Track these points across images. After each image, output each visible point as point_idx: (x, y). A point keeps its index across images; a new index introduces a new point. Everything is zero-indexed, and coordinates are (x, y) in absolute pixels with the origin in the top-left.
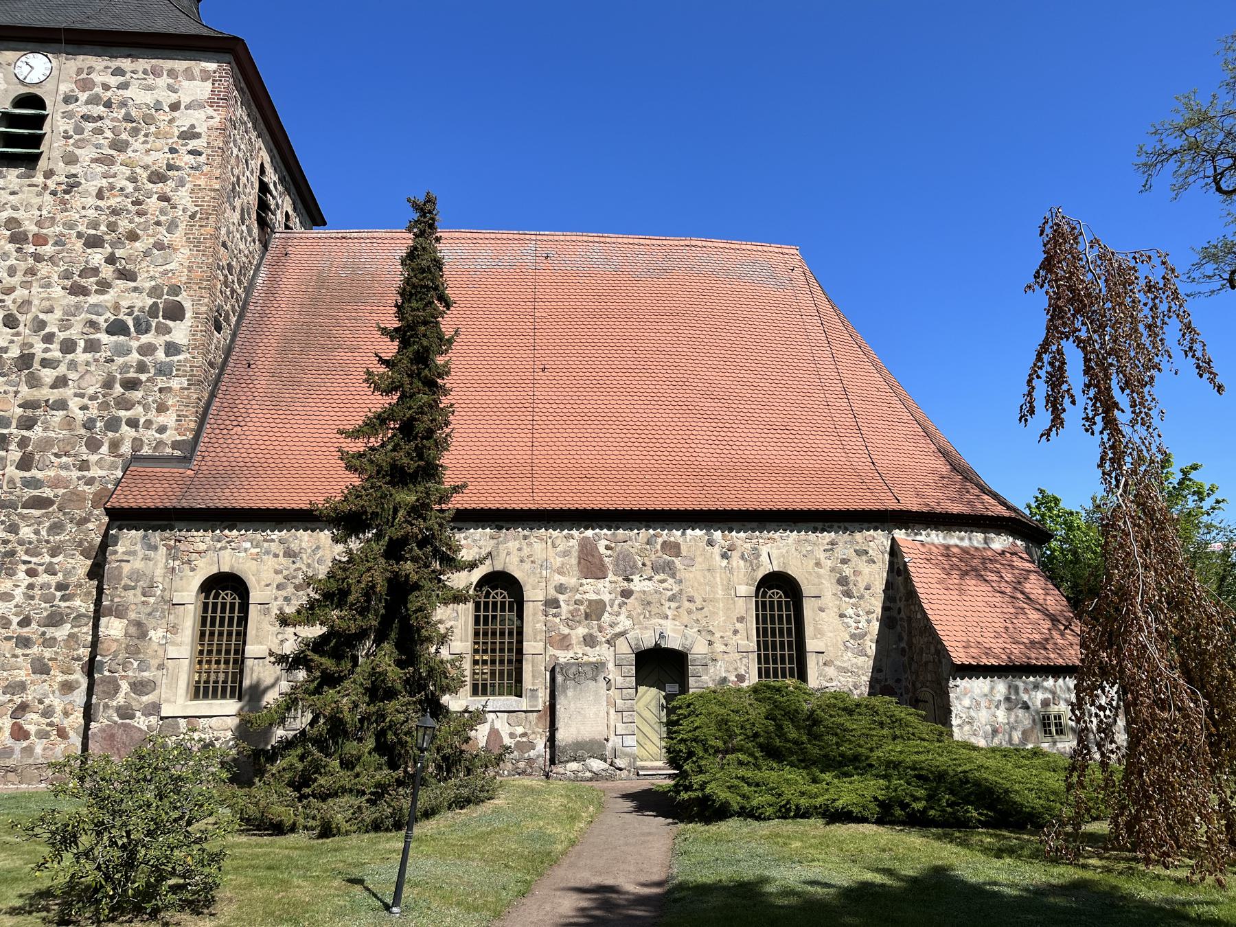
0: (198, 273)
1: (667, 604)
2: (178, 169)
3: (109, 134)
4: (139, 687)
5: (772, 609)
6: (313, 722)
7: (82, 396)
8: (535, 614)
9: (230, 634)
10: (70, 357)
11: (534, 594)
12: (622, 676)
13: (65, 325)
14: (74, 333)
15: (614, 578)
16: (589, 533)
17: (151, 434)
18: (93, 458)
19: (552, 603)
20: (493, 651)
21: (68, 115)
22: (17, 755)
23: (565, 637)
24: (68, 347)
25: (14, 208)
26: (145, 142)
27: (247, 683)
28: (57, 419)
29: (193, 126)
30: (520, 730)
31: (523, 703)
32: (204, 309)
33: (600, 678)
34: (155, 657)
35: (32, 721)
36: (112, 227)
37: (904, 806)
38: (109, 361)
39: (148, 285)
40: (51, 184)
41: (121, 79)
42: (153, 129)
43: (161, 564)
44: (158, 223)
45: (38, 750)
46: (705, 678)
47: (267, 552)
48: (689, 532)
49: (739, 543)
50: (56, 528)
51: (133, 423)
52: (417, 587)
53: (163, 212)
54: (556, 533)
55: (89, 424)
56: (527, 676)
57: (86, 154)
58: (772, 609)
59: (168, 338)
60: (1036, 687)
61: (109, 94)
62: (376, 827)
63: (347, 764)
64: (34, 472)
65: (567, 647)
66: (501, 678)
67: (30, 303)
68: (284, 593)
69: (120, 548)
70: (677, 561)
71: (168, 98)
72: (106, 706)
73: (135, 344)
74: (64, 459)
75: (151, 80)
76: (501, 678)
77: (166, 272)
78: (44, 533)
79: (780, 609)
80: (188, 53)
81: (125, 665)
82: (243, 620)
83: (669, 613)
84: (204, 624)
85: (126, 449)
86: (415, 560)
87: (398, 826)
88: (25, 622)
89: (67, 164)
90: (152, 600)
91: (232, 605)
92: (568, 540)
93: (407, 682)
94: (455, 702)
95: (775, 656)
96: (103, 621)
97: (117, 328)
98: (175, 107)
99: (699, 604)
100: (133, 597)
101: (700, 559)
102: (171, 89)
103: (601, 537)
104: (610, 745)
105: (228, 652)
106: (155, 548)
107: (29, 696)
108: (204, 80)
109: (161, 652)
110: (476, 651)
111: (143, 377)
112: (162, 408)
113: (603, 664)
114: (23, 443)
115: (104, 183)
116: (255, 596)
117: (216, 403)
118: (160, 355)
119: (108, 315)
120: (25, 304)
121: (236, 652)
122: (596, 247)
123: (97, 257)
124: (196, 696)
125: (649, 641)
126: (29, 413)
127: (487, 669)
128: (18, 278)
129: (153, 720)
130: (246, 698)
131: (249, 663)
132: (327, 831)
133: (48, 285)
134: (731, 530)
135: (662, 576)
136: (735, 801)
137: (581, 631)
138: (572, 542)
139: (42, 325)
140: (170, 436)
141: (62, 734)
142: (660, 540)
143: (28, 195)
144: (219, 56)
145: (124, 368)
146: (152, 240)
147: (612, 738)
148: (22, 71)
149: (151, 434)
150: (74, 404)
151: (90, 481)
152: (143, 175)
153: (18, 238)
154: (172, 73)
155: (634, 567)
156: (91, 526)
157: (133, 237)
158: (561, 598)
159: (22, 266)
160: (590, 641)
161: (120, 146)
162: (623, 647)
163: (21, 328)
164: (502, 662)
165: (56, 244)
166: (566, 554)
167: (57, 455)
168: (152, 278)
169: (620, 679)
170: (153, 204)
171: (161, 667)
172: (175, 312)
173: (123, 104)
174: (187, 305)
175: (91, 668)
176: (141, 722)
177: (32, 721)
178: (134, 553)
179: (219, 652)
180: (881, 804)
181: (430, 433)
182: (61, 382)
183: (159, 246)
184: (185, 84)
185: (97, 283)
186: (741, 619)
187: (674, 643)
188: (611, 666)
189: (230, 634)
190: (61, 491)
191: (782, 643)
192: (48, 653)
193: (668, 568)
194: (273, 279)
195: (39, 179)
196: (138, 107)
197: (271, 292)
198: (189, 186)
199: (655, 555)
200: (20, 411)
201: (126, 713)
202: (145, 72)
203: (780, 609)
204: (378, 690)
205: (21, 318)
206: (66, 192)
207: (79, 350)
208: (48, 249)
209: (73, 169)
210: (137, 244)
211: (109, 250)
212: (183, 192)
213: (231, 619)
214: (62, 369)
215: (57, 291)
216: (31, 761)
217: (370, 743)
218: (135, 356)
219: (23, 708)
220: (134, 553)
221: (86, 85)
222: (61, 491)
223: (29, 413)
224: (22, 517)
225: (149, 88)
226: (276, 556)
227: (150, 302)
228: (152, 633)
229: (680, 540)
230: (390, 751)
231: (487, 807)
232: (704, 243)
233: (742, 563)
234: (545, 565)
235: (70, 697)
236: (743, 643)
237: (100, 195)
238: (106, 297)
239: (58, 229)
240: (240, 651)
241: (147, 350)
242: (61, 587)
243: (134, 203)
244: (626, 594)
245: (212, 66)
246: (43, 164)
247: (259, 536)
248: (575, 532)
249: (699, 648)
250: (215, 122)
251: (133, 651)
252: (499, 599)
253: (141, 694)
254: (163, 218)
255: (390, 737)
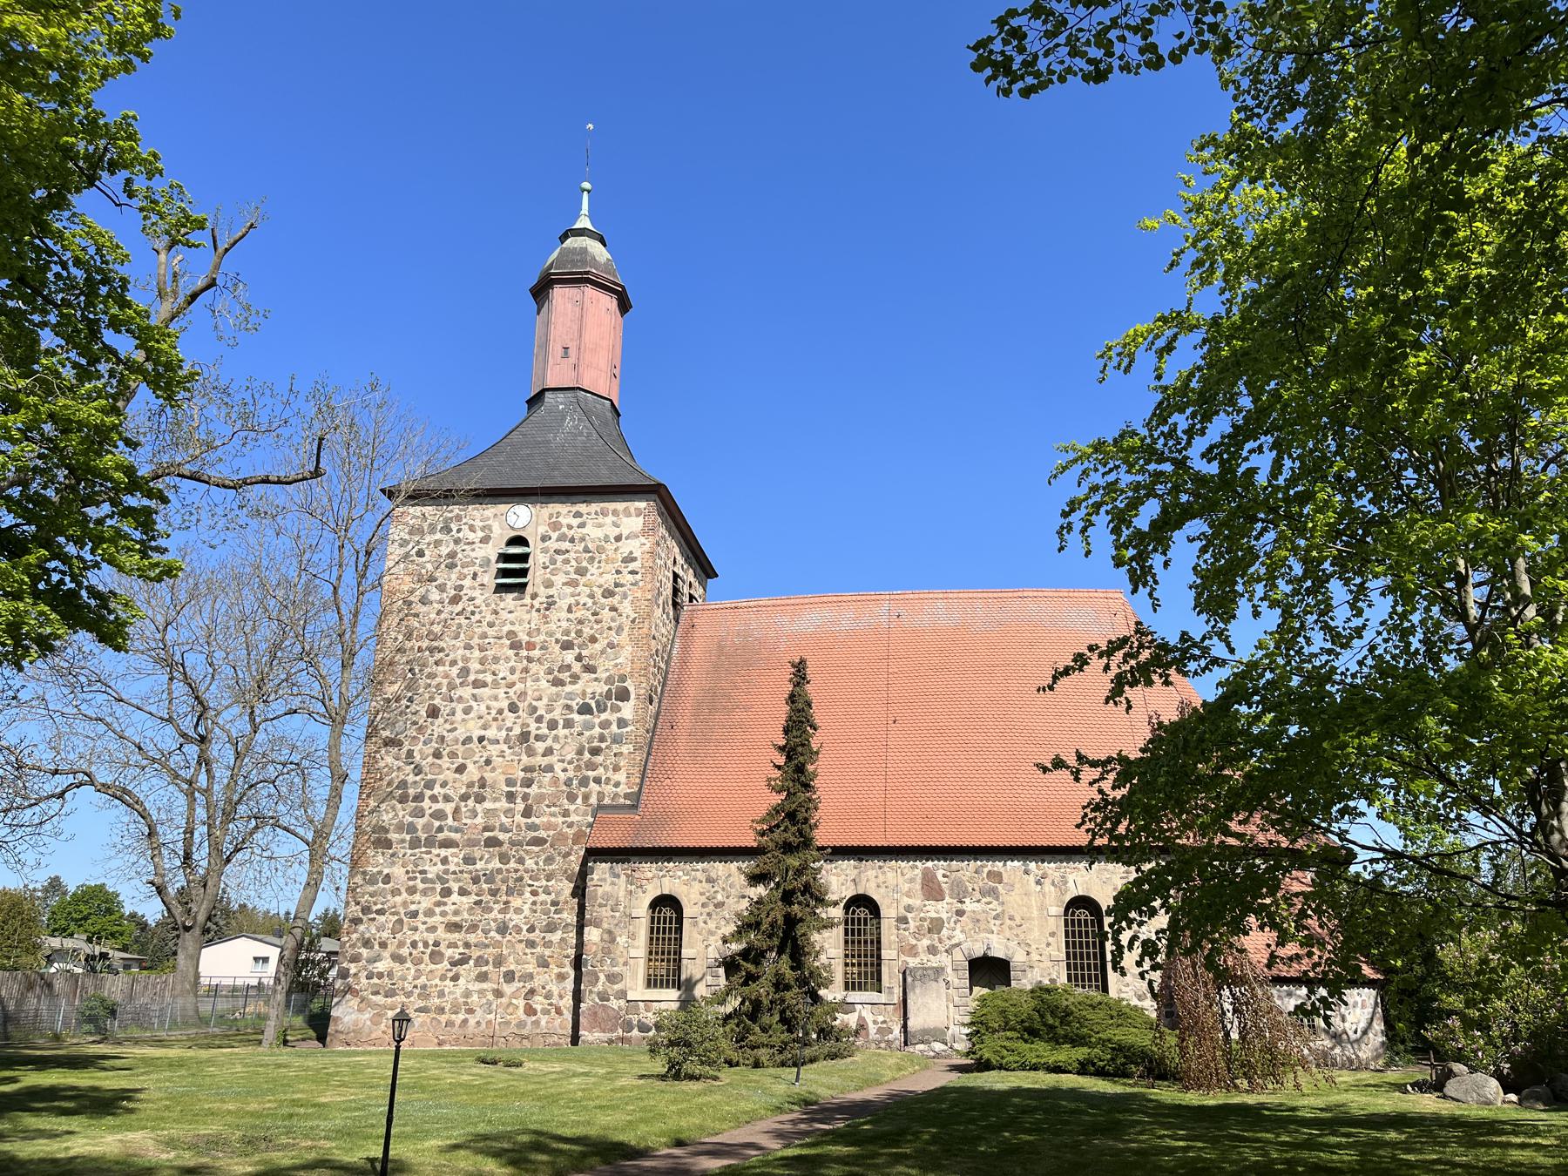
0: (638, 665)
1: (993, 922)
2: (622, 586)
3: (573, 563)
4: (612, 978)
5: (1080, 926)
6: (742, 1003)
7: (563, 761)
8: (890, 928)
9: (670, 939)
10: (554, 732)
11: (888, 912)
12: (961, 979)
13: (550, 710)
14: (556, 714)
15: (950, 901)
16: (930, 864)
17: (609, 789)
18: (572, 807)
19: (903, 920)
20: (859, 956)
21: (545, 551)
22: (529, 1026)
23: (913, 947)
24: (553, 725)
25: (512, 623)
26: (599, 568)
27: (683, 977)
28: (547, 779)
29: (631, 553)
30: (881, 1018)
31: (883, 998)
32: (642, 691)
33: (941, 980)
34: (621, 957)
35: (539, 1002)
36: (579, 633)
37: (1094, 1064)
38: (580, 734)
39: (605, 675)
40: (536, 603)
41: (579, 520)
42: (604, 556)
43: (623, 888)
44: (610, 628)
45: (543, 1023)
46: (1024, 981)
47: (695, 879)
48: (1009, 863)
49: (1050, 872)
50: (549, 860)
51: (597, 781)
52: (801, 920)
53: (613, 620)
54: (903, 864)
55: (568, 783)
56: (885, 977)
57: (559, 579)
58: (1080, 926)
59: (619, 715)
60: (1290, 994)
61: (572, 532)
62: (783, 1064)
63: (764, 1030)
64: (533, 819)
65: (915, 955)
66: (866, 978)
67: (525, 693)
68: (707, 910)
69: (595, 876)
70: (1000, 887)
71: (614, 532)
72: (591, 992)
73: (597, 721)
74: (553, 809)
75: (601, 519)
76: (866, 978)
77: (616, 665)
78: (541, 863)
79: (1086, 926)
80: (625, 496)
81: (601, 962)
82: (679, 930)
83: (994, 928)
84: (652, 932)
85: (593, 800)
86: (800, 903)
87: (795, 1065)
88: (531, 929)
89: (546, 587)
90: (617, 914)
91: (671, 918)
92: (914, 869)
93: (797, 980)
94: (829, 994)
95: (1082, 964)
96: (586, 929)
97: (585, 709)
98: (618, 539)
99: (1018, 921)
100: (605, 912)
101: (1017, 886)
102: (616, 525)
103: (939, 867)
104: (950, 1031)
105: (669, 953)
106: (618, 876)
107: (536, 984)
108: (638, 515)
109: (625, 953)
110: (846, 956)
111: (603, 745)
112: (616, 769)
113: (943, 969)
114: (525, 797)
115: (572, 600)
116: (687, 912)
117: (651, 760)
118: (614, 727)
119: (578, 700)
120: (523, 694)
121: (675, 954)
122: (940, 604)
123: (569, 656)
124: (649, 985)
125: (978, 952)
126: (529, 775)
127: (855, 970)
128: (517, 675)
129: (622, 1002)
130: (683, 988)
131: (684, 962)
132: (757, 1065)
133: (538, 680)
134: (1043, 862)
135: (988, 899)
136: (994, 1059)
137: (926, 942)
138: (917, 871)
139: (535, 709)
140: (623, 789)
141: (559, 1012)
142: (986, 870)
143: (521, 613)
144: (647, 496)
145: (591, 739)
146: (606, 641)
147: (952, 1026)
148: (512, 519)
149: (609, 789)
150: (558, 767)
151: (570, 825)
152: (598, 592)
153: (515, 646)
154: (615, 513)
155: (966, 891)
156: (572, 858)
157: (593, 640)
158: (909, 916)
159: (520, 666)
160: (932, 950)
161: (581, 572)
162: (958, 955)
163: (520, 713)
164: (866, 965)
165: (541, 648)
166: (912, 880)
167: (548, 806)
168: (607, 670)
169: (956, 981)
170: (606, 614)
171: (625, 964)
172: (623, 695)
173: (583, 539)
174: (631, 689)
175: (578, 963)
176: (614, 1003)
177: (539, 1002)
178: (605, 880)
179: (663, 953)
180: (1080, 1063)
181: (806, 820)
182: (549, 752)
183: (611, 645)
184: (625, 520)
185: (571, 676)
186: (1053, 934)
187: (998, 952)
188: (949, 970)
189: (670, 939)
190: (551, 833)
191: (1088, 954)
192: (547, 952)
193: (993, 893)
194: (685, 649)
195: (527, 600)
196: (593, 541)
197: (684, 661)
198: (630, 598)
199: (983, 881)
200: (522, 774)
201: (604, 997)
202: (596, 513)
203: (1086, 926)
204: (780, 985)
205: (521, 705)
206: (547, 609)
207: (560, 726)
208: (536, 653)
209: (551, 592)
210: (596, 645)
211: (577, 651)
212: (626, 603)
213: (670, 929)
214: (549, 742)
215: (544, 684)
216: (538, 1031)
217: (777, 1017)
218: (597, 730)
219: (532, 992)
220: (605, 880)
221: (556, 526)
222: (551, 833)
223: (529, 775)
224: (527, 852)
225: (600, 526)
226: (701, 882)
227: (606, 688)
228: (618, 939)
229: (1002, 870)
230: (788, 1023)
231: (849, 1060)
232: (1035, 594)
233: (1052, 888)
234: (896, 889)
235: (563, 985)
236: (1055, 953)
237: (570, 610)
238: (577, 686)
239: (542, 637)
240: (678, 952)
241: (605, 725)
242: (554, 903)
243: (593, 614)
244: (960, 913)
245: (643, 505)
246: (529, 589)
247: (688, 866)
248: (918, 863)
249: (1018, 958)
250: (647, 548)
251: (607, 952)
252: (862, 916)
253: (613, 983)
254: (613, 624)
255: (788, 1013)
